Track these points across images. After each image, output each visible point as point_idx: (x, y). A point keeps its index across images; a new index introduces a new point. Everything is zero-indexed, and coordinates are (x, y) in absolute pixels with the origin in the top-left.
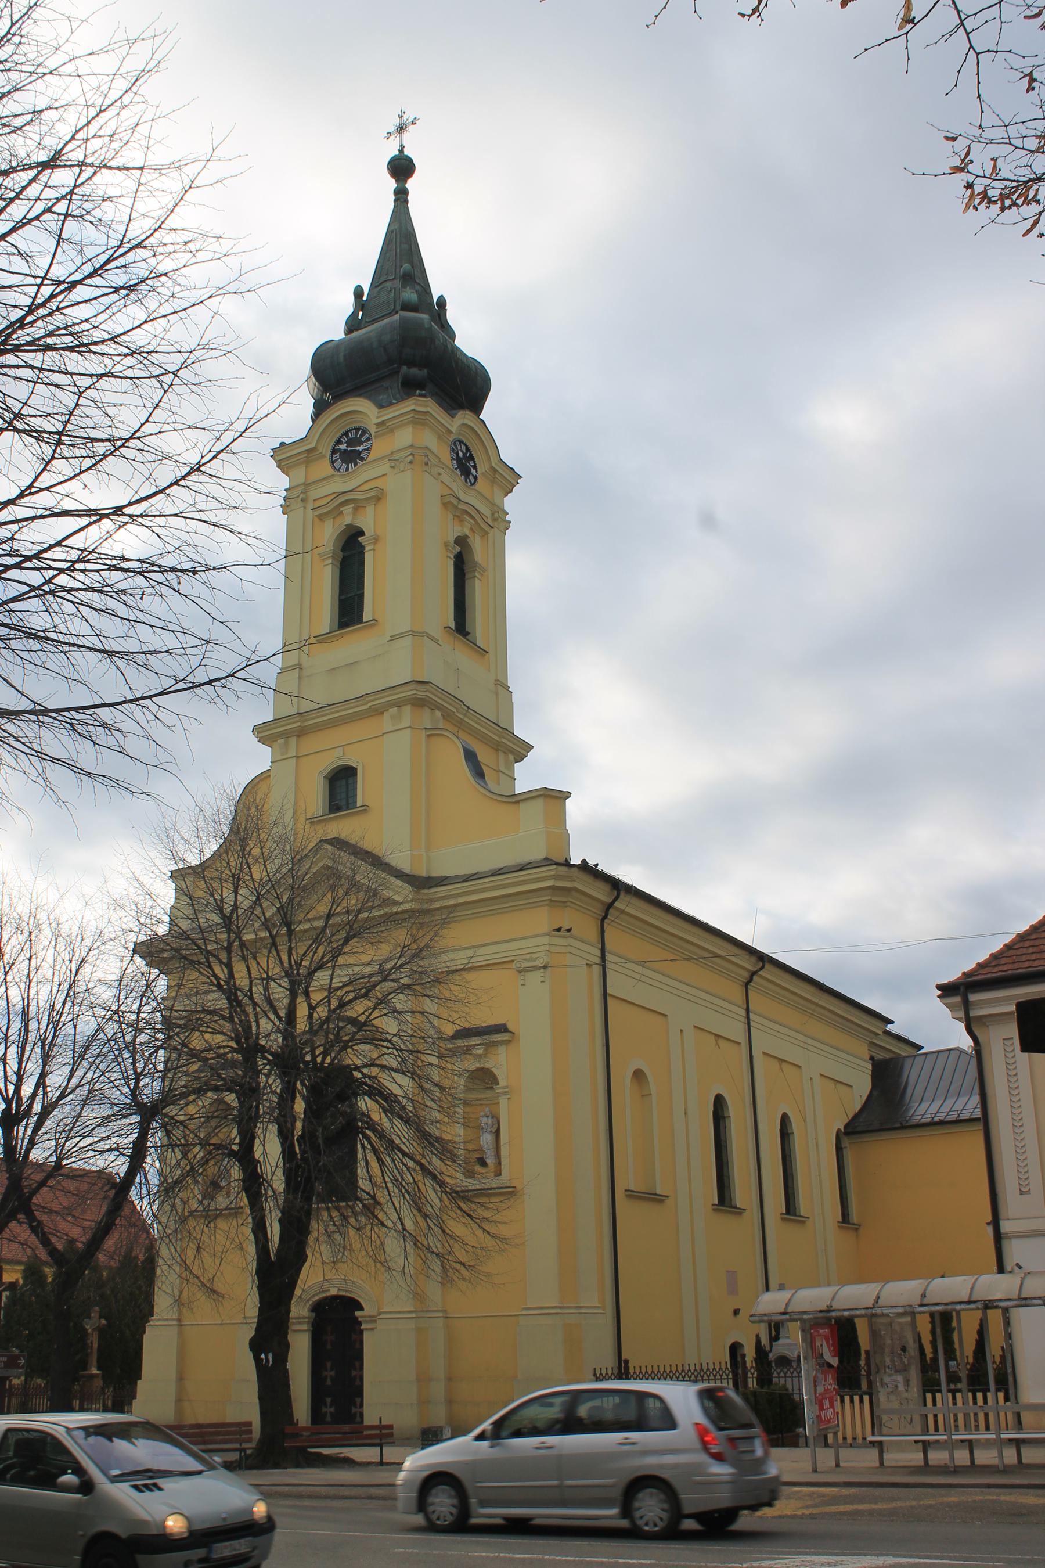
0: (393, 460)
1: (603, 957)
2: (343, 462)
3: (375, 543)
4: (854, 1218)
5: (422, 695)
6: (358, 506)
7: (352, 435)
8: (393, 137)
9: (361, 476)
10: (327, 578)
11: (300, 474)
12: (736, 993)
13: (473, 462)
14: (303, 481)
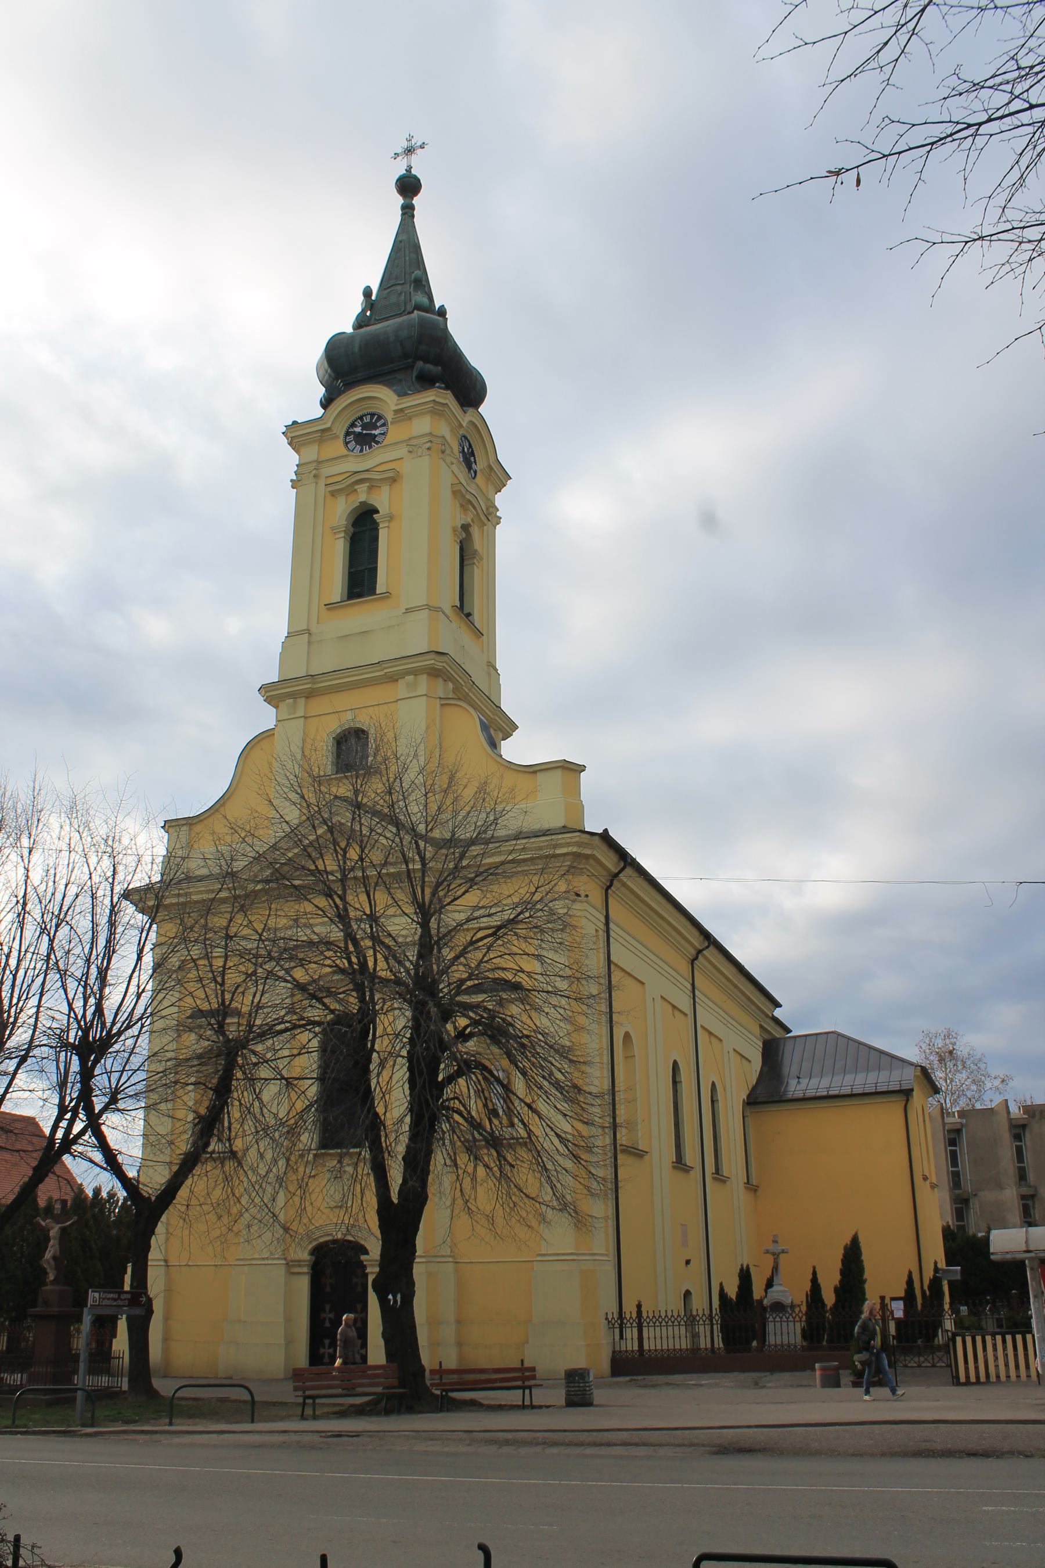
0: (411, 444)
1: (607, 924)
2: (357, 443)
3: (389, 521)
4: (754, 1181)
5: (439, 665)
6: (373, 485)
7: (367, 419)
8: (400, 158)
9: (375, 459)
10: (338, 551)
11: (312, 453)
12: (684, 968)
13: (475, 460)
14: (315, 458)
